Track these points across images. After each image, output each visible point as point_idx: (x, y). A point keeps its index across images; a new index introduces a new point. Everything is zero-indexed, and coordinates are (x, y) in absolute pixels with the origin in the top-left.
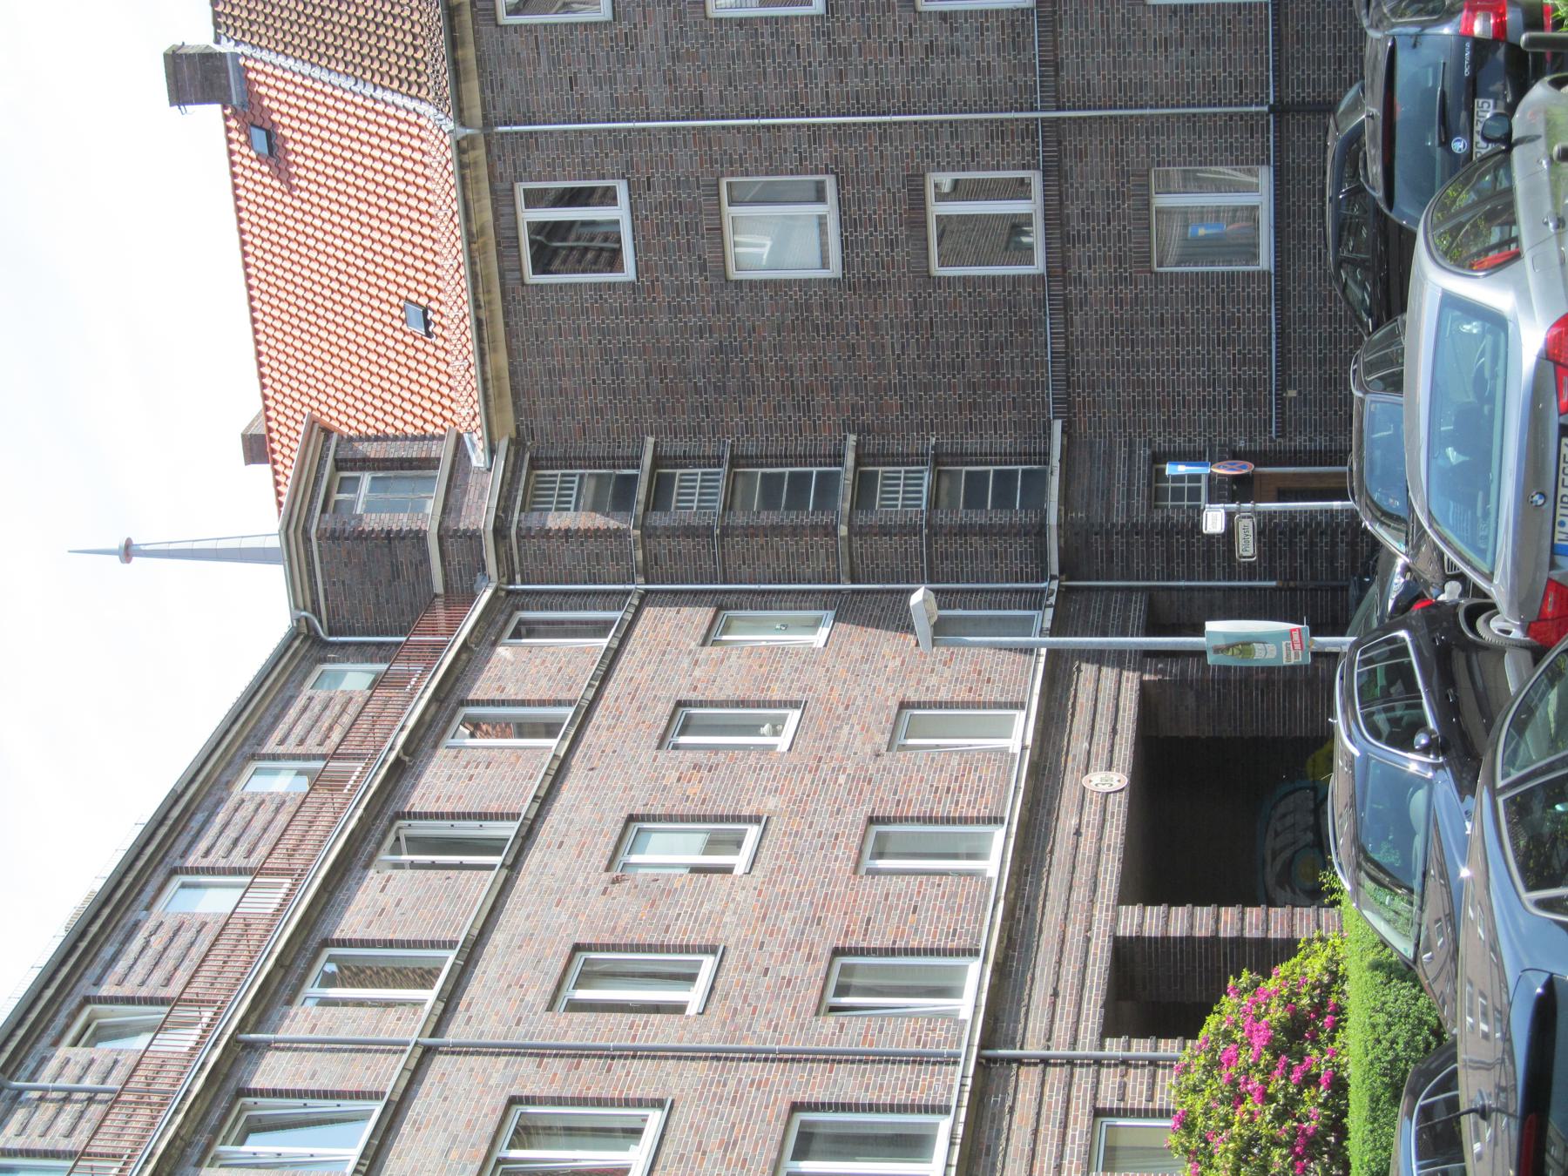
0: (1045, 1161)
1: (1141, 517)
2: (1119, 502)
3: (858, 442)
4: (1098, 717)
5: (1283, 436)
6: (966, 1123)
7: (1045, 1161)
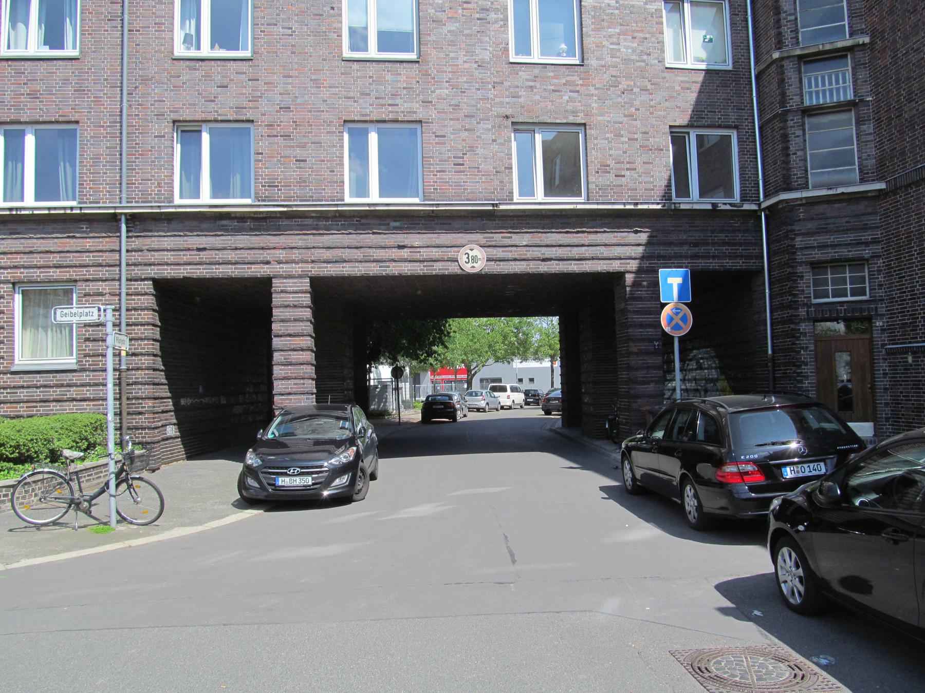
0: (5, 261)
1: (800, 257)
2: (812, 241)
3: (864, 44)
4: (569, 248)
5: (888, 354)
6: (33, 214)
7: (5, 261)
